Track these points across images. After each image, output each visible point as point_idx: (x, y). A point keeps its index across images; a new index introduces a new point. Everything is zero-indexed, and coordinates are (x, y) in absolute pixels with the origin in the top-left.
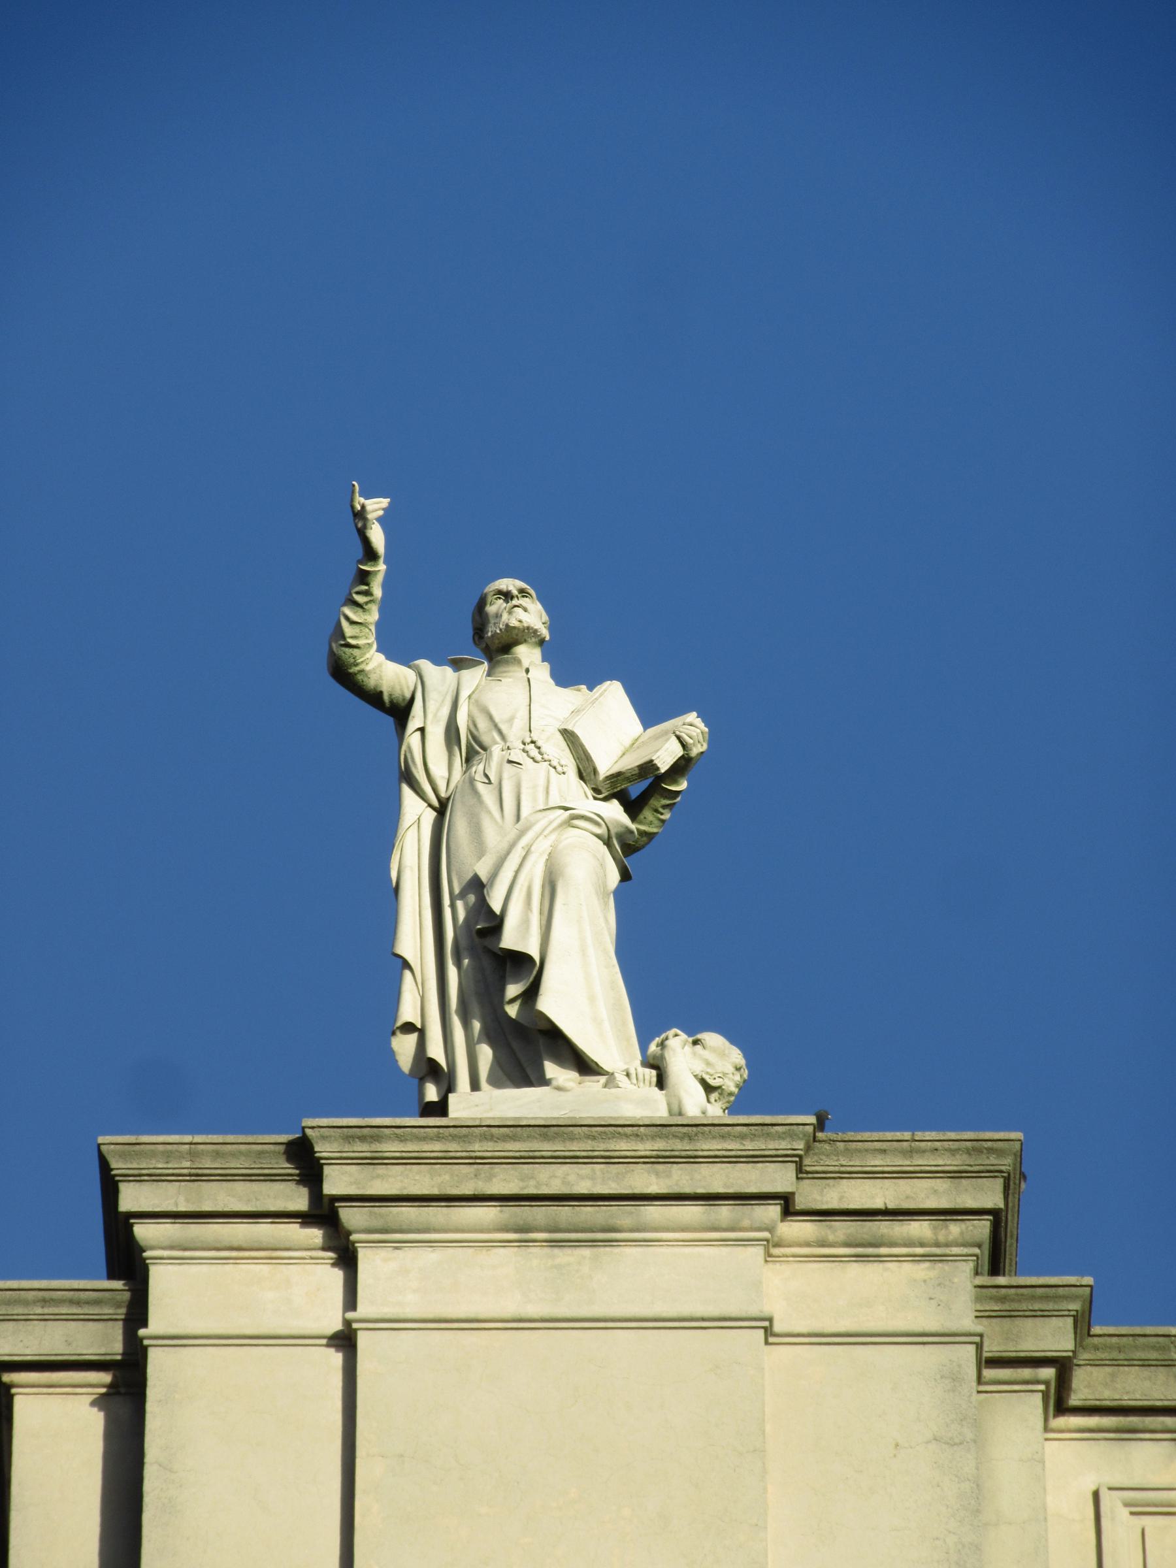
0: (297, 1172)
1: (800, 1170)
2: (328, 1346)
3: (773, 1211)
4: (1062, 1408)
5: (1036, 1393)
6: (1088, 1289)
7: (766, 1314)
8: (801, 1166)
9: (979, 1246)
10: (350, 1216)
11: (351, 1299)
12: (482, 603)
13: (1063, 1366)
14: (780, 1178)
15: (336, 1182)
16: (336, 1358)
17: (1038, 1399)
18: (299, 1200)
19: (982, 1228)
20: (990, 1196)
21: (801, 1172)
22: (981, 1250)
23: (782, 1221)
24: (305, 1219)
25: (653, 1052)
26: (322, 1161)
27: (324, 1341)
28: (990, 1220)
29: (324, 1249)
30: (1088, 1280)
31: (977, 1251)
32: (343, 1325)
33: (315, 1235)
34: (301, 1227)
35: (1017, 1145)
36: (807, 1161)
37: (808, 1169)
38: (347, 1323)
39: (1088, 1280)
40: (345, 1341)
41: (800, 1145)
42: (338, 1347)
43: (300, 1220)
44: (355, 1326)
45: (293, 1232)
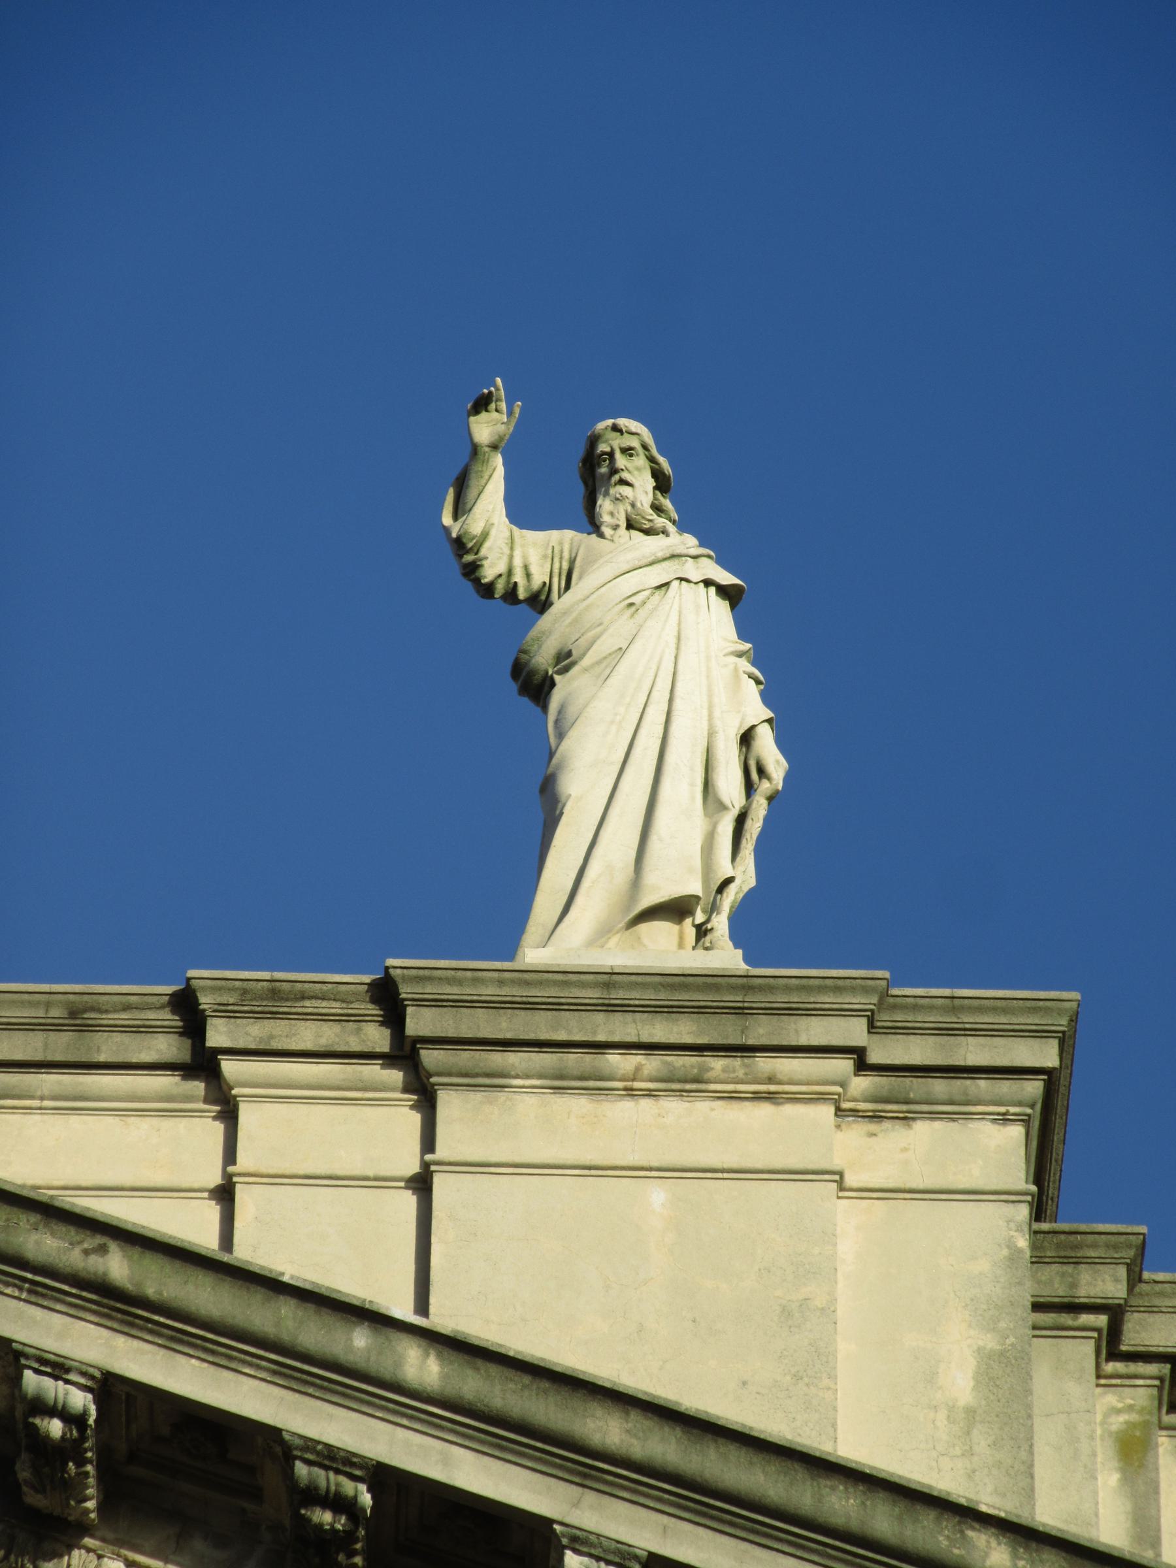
0: (382, 1013)
1: (872, 1027)
2: (406, 1188)
3: (844, 1065)
4: (1114, 1354)
5: (1089, 1340)
6: (1141, 1237)
7: (837, 1168)
8: (872, 1022)
9: (1032, 1106)
10: (430, 1057)
11: (428, 1142)
12: (594, 440)
13: (1116, 1313)
14: (854, 1032)
15: (418, 1023)
16: (409, 1200)
17: (1091, 1344)
18: (378, 1037)
19: (1034, 1088)
20: (1047, 1055)
21: (873, 1027)
22: (1034, 1112)
23: (856, 1075)
24: (388, 1060)
26: (406, 1003)
27: (402, 1184)
28: (1044, 1080)
29: (406, 1090)
30: (1143, 1229)
31: (1029, 1111)
32: (421, 1168)
33: (396, 1076)
34: (382, 1069)
35: (1075, 1005)
36: (877, 1017)
37: (879, 1024)
38: (426, 1166)
40: (422, 1184)
41: (875, 1000)
42: (416, 1190)
43: (380, 1062)
44: (433, 1168)
45: (373, 1071)
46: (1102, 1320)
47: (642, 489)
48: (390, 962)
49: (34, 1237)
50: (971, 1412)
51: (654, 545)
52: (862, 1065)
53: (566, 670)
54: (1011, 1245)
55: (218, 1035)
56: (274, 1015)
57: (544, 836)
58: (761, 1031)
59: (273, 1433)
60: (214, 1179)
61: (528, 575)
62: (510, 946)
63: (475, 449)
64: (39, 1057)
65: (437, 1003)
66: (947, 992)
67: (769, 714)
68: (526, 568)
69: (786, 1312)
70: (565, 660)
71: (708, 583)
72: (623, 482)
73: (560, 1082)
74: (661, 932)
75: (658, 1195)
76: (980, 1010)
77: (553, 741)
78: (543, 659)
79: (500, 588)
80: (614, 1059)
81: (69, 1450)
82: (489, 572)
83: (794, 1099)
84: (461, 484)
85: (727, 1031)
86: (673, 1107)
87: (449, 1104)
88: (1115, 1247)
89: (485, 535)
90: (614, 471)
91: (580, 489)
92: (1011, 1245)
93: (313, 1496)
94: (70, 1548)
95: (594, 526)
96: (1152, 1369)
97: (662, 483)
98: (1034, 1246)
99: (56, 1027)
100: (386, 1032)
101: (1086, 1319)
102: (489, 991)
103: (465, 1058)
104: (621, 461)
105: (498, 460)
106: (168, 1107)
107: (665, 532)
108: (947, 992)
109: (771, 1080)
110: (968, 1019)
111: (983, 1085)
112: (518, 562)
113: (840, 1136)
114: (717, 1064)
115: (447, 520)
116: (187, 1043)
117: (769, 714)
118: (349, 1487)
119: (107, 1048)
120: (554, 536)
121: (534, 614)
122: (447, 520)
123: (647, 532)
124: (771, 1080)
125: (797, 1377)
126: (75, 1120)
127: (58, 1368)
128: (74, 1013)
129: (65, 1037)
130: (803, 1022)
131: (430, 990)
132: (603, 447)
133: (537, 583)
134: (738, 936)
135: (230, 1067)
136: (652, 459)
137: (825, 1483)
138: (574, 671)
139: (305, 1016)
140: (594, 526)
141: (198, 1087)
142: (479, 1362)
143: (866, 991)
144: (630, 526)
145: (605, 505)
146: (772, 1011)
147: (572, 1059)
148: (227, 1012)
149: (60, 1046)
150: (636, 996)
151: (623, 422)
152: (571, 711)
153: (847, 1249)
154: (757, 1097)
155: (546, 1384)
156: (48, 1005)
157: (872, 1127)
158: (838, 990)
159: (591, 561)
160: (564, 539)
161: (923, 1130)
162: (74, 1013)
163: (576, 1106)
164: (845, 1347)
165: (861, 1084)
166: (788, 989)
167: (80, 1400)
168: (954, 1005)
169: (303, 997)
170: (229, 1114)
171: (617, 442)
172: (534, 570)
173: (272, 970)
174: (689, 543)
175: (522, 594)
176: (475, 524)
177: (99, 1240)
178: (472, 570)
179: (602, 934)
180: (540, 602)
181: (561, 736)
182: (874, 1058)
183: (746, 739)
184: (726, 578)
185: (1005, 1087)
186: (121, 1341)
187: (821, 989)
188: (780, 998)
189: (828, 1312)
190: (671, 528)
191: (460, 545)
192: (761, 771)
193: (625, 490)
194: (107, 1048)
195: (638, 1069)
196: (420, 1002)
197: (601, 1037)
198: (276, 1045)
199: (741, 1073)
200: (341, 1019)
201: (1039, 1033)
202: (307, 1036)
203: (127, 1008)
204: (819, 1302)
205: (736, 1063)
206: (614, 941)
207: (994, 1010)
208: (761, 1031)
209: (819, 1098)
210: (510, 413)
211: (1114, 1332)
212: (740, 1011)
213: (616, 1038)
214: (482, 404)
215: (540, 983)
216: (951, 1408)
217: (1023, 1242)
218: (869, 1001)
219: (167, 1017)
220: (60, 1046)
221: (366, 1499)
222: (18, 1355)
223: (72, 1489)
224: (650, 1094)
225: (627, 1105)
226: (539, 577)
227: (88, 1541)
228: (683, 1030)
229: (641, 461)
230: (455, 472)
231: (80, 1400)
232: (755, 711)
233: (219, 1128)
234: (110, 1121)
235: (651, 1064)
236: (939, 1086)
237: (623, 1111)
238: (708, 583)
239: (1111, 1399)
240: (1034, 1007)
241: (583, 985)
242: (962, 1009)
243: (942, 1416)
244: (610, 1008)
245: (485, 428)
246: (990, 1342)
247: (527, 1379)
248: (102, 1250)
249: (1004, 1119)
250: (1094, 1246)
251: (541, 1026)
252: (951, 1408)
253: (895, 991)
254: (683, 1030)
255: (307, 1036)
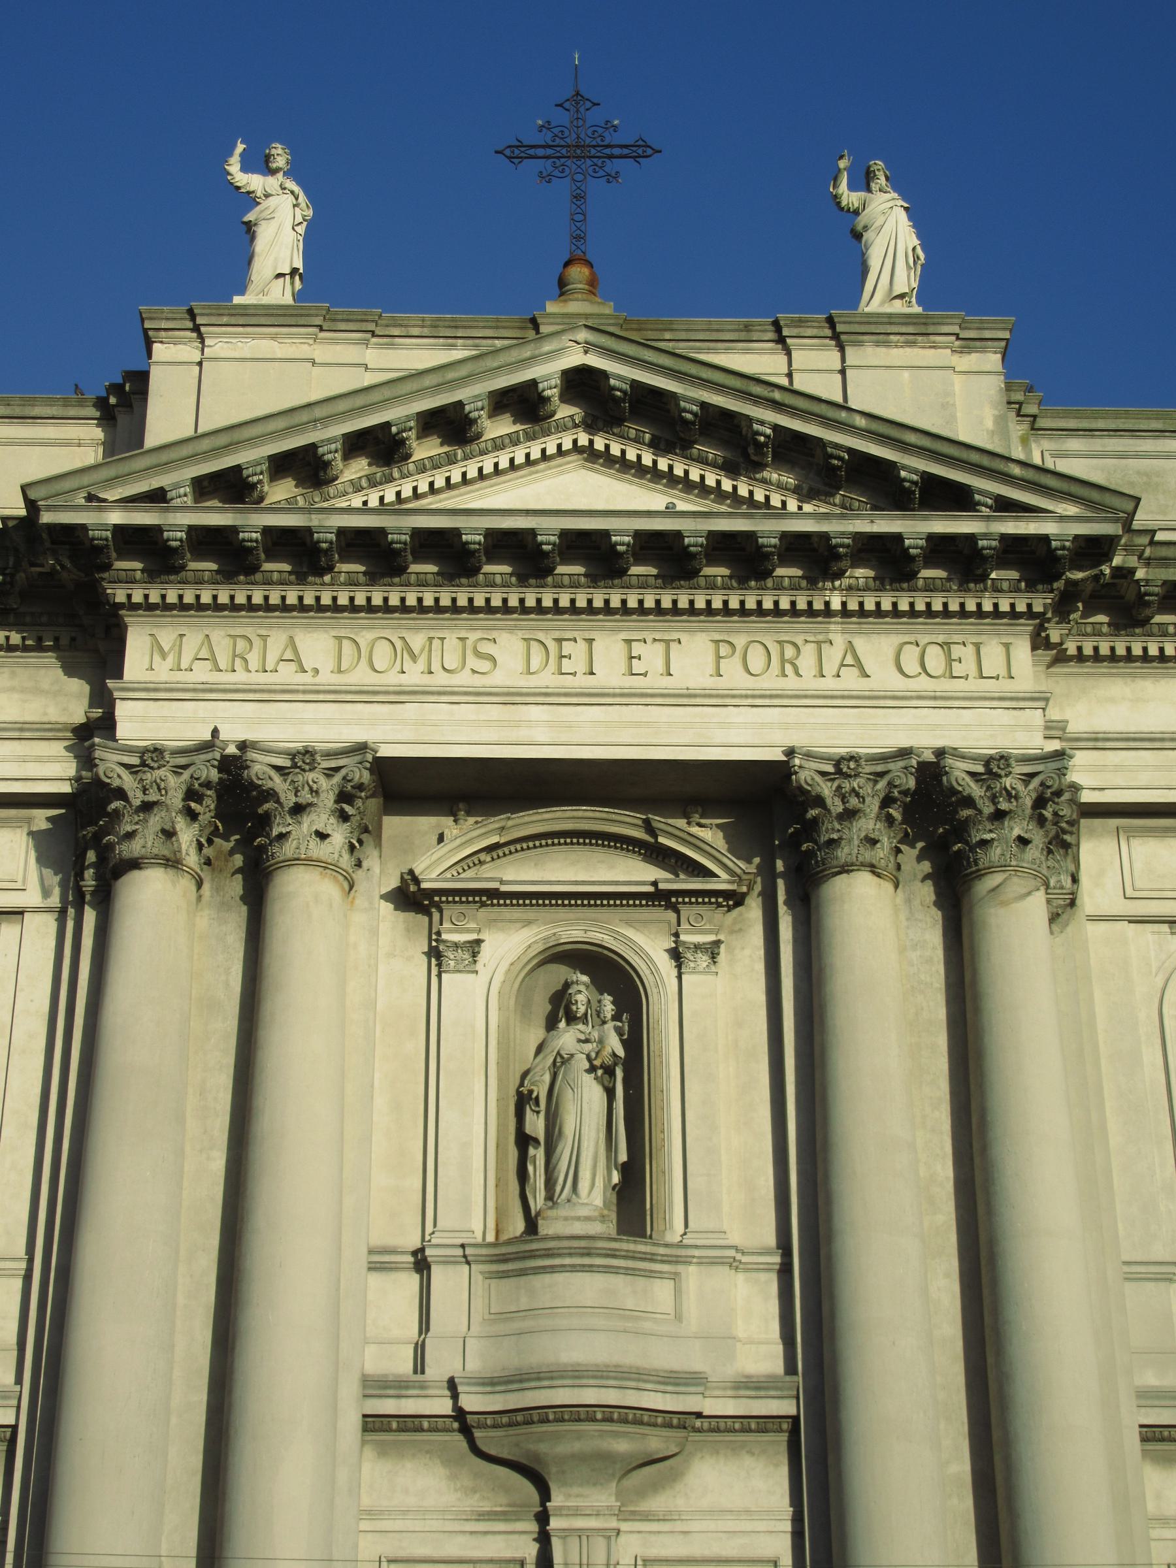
3: (953, 338)
10: (843, 337)
11: (843, 360)
12: (869, 167)
13: (1020, 404)
14: (956, 329)
15: (840, 328)
16: (839, 377)
18: (828, 332)
19: (1003, 344)
20: (1007, 335)
24: (831, 338)
25: (528, 923)
33: (833, 343)
39: (1042, 394)
40: (843, 372)
45: (827, 341)
46: (1017, 406)
47: (882, 181)
48: (832, 312)
49: (754, 388)
50: (993, 432)
51: (888, 196)
52: (958, 338)
53: (866, 231)
54: (1000, 386)
55: (785, 332)
56: (800, 327)
57: (862, 276)
58: (931, 329)
59: (821, 439)
60: (786, 371)
61: (853, 205)
62: (856, 308)
63: (839, 170)
64: (737, 339)
65: (844, 323)
66: (798, 316)
67: (919, 242)
68: (852, 203)
69: (943, 405)
70: (866, 228)
71: (902, 206)
72: (878, 179)
73: (878, 344)
74: (898, 302)
75: (906, 374)
76: (988, 323)
77: (864, 250)
78: (859, 228)
79: (846, 208)
80: (892, 337)
81: (765, 445)
82: (844, 203)
83: (940, 348)
84: (835, 179)
85: (922, 329)
86: (908, 350)
87: (849, 351)
88: (1021, 386)
89: (843, 194)
90: (875, 175)
91: (865, 181)
92: (1000, 386)
93: (832, 456)
94: (763, 471)
95: (869, 190)
96: (1029, 419)
97: (887, 179)
98: (1005, 386)
99: (742, 331)
100: (830, 331)
101: (1013, 406)
102: (858, 319)
103: (853, 337)
104: (877, 173)
105: (846, 173)
106: (772, 352)
107: (889, 192)
108: (798, 316)
109: (934, 342)
110: (986, 325)
111: (990, 343)
112: (850, 201)
113: (952, 358)
114: (920, 338)
115: (831, 190)
116: (777, 334)
117: (919, 242)
118: (842, 454)
119: (755, 336)
120: (859, 194)
121: (854, 216)
122: (831, 190)
123: (885, 192)
124: (934, 342)
125: (947, 423)
126: (747, 356)
127: (762, 423)
128: (746, 326)
129: (744, 333)
130: (942, 327)
131: (843, 319)
132: (872, 169)
133: (855, 207)
134: (919, 303)
135: (789, 341)
136: (884, 172)
137: (970, 451)
138: (870, 231)
139: (808, 327)
140: (869, 190)
141: (780, 346)
142: (876, 420)
143: (958, 318)
144: (880, 190)
145: (873, 185)
146: (934, 324)
147: (881, 337)
148: (787, 326)
149: (743, 336)
150: (897, 320)
151: (877, 162)
152: (870, 242)
153: (957, 388)
154: (931, 347)
155: (894, 426)
156: (739, 325)
157: (960, 355)
158: (951, 318)
159: (871, 200)
160: (862, 194)
161: (974, 355)
162: (746, 326)
163: (882, 351)
164: (959, 414)
165: (958, 343)
166: (938, 318)
167: (769, 431)
168: (982, 322)
169: (808, 321)
170: (789, 354)
171: (876, 168)
172: (854, 203)
173: (453, 314)
174: (895, 195)
175: (851, 210)
176: (840, 192)
177: (772, 388)
178: (839, 203)
179: (882, 303)
180: (856, 213)
181: (867, 249)
182: (961, 336)
183: (914, 249)
184: (906, 205)
185: (996, 344)
186: (778, 415)
187: (947, 318)
188: (936, 321)
189: (954, 405)
190: (892, 191)
191: (836, 196)
192: (918, 258)
193: (879, 181)
194: (755, 336)
195: (899, 340)
196: (839, 322)
197: (889, 332)
198: (802, 335)
199: (926, 341)
200: (820, 327)
201: (1004, 329)
202: (809, 332)
203: (760, 325)
204: (951, 402)
205: (925, 338)
206: (886, 305)
207: (992, 323)
208: (931, 329)
209: (947, 347)
210: (849, 160)
211: (1019, 410)
212: (925, 324)
213: (893, 332)
214: (841, 157)
215: (872, 317)
216: (987, 431)
217: (1003, 386)
218: (959, 321)
219: (772, 328)
220: (743, 336)
221: (847, 457)
222: (751, 419)
223: (764, 455)
224: (902, 347)
225: (896, 350)
226: (856, 205)
227: (768, 469)
228: (911, 329)
229: (882, 173)
230: (834, 175)
231: (769, 431)
232: (916, 242)
233: (786, 357)
234: (756, 356)
235: (902, 338)
236: (978, 344)
237: (895, 351)
238: (902, 206)
239: (1018, 427)
240: (1003, 322)
241: (883, 317)
242: (983, 323)
243: (985, 433)
244: (891, 323)
245: (842, 164)
246: (996, 413)
247: (888, 424)
248: (773, 391)
249: (995, 353)
250: (1015, 386)
251: (872, 329)
252: (987, 431)
253: (383, 315)
254: (911, 329)
255: (809, 332)
